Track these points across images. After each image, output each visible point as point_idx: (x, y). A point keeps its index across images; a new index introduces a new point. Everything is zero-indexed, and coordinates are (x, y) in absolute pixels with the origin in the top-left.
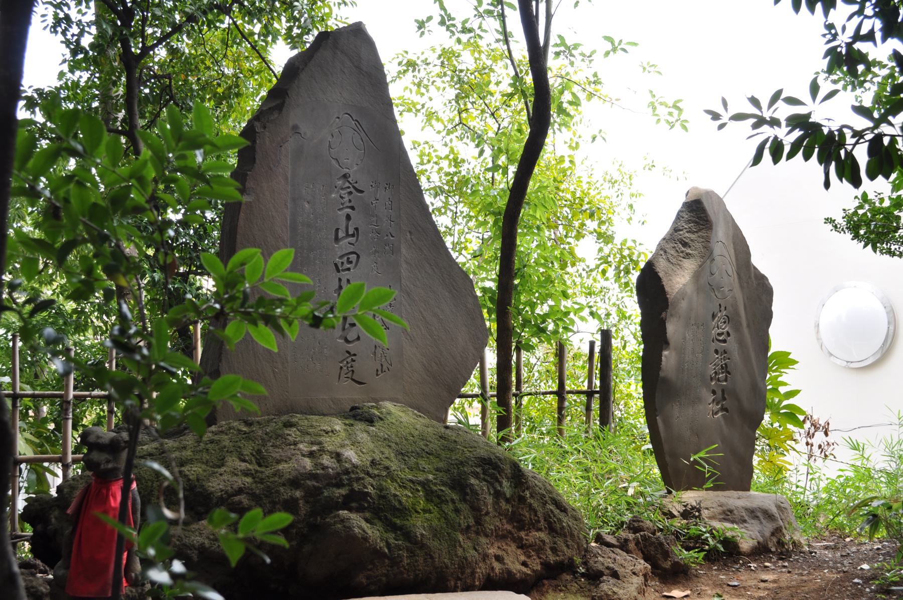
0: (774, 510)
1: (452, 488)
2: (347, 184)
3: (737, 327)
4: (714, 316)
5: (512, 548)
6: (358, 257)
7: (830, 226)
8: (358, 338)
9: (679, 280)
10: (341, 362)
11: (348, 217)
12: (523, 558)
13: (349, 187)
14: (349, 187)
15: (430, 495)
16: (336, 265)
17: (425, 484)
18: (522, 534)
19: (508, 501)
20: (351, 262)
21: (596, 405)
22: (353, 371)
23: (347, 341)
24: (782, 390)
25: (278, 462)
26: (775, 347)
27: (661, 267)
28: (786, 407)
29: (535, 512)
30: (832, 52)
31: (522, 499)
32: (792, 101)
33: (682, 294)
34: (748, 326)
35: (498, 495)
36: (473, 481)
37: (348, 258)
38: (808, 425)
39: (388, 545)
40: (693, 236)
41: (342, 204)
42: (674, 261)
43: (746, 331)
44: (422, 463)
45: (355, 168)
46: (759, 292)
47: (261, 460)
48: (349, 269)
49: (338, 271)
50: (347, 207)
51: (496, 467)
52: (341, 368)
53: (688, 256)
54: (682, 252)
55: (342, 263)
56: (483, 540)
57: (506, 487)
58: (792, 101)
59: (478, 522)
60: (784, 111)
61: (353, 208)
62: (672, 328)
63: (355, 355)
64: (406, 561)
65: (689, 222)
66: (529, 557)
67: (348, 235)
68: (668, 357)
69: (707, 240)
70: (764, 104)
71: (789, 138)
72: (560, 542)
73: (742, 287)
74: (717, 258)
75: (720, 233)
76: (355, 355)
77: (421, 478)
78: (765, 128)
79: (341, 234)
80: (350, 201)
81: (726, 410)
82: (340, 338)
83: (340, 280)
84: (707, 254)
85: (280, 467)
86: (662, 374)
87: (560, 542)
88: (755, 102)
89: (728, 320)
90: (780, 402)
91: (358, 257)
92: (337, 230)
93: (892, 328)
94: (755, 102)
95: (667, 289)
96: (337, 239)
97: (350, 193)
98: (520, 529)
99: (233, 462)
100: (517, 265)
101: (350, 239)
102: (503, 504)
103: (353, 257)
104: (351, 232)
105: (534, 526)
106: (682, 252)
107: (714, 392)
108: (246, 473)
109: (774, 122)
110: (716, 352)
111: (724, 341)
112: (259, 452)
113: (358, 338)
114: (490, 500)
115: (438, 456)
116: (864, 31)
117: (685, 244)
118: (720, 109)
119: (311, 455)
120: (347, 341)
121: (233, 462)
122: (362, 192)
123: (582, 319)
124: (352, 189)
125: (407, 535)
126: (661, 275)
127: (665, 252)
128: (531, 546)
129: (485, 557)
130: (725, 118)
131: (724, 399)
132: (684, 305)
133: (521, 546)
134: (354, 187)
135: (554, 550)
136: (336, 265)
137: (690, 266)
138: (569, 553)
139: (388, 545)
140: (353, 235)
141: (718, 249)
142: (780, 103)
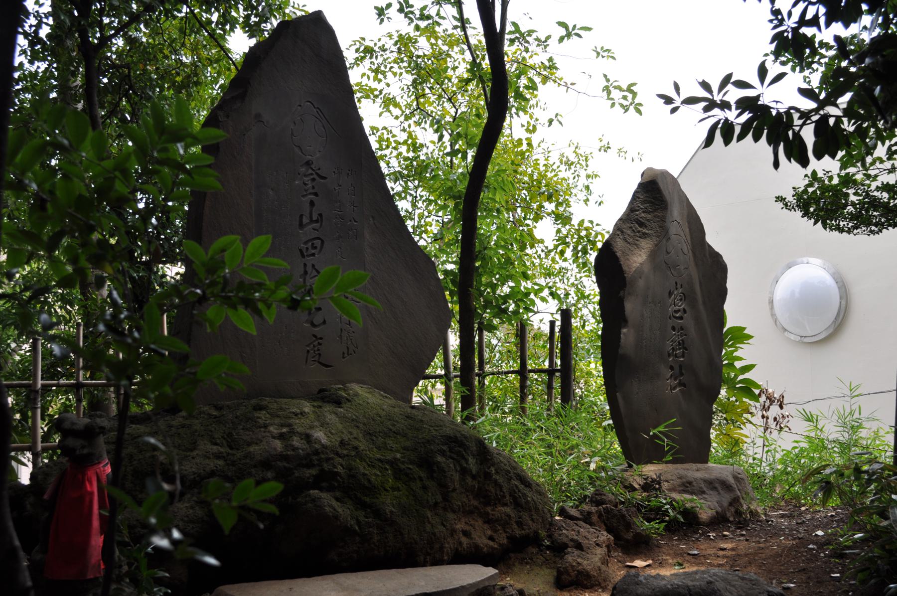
0: (732, 481)
1: (420, 466)
2: (310, 171)
3: (693, 304)
4: (670, 294)
5: (480, 523)
6: (323, 242)
7: (781, 205)
8: (324, 322)
9: (637, 259)
10: (308, 346)
11: (312, 203)
12: (489, 533)
13: (312, 174)
14: (312, 174)
15: (399, 474)
16: (301, 251)
17: (393, 463)
18: (489, 509)
19: (474, 477)
20: (315, 248)
21: (557, 384)
22: (320, 354)
23: (313, 325)
24: (738, 364)
25: (249, 444)
26: (730, 323)
27: (619, 245)
28: (741, 381)
29: (501, 487)
30: (778, 38)
31: (488, 475)
32: (742, 85)
33: (639, 272)
34: (704, 303)
35: (464, 471)
36: (440, 459)
37: (313, 244)
38: (763, 398)
39: (358, 522)
40: (649, 216)
41: (306, 191)
42: (631, 240)
43: (701, 307)
44: (390, 443)
45: (318, 155)
46: (713, 270)
47: (233, 444)
48: (313, 255)
49: (303, 256)
50: (310, 194)
51: (462, 444)
52: (308, 351)
53: (644, 236)
54: (639, 232)
55: (307, 249)
56: (451, 516)
57: (472, 464)
58: (742, 85)
59: (446, 498)
60: (734, 94)
61: (316, 194)
62: (631, 307)
63: (321, 338)
64: (376, 538)
65: (644, 202)
66: (496, 531)
67: (312, 221)
68: (627, 335)
69: (663, 220)
70: (715, 88)
71: (739, 119)
72: (525, 517)
73: (697, 265)
74: (673, 237)
75: (676, 212)
76: (321, 338)
77: (389, 456)
78: (716, 111)
79: (305, 220)
80: (313, 188)
81: (684, 385)
82: (307, 322)
83: (305, 265)
84: (663, 233)
85: (251, 449)
86: (621, 351)
87: (525, 517)
88: (705, 86)
89: (684, 297)
90: (736, 376)
91: (323, 242)
92: (301, 216)
93: (844, 303)
94: (705, 86)
95: (625, 268)
96: (301, 225)
97: (313, 180)
98: (487, 504)
99: (205, 446)
100: (478, 247)
101: (314, 225)
102: (469, 480)
103: (318, 243)
104: (315, 218)
105: (500, 501)
107: (672, 368)
108: (218, 456)
109: (725, 105)
110: (673, 329)
111: (681, 318)
112: (230, 435)
113: (324, 322)
114: (456, 477)
115: (405, 436)
116: (809, 16)
117: (641, 224)
118: (672, 94)
119: (281, 436)
120: (313, 325)
121: (205, 446)
122: (325, 178)
123: (543, 300)
124: (315, 176)
125: (377, 513)
126: (619, 254)
128: (497, 520)
129: (453, 532)
130: (678, 102)
131: (682, 374)
132: (641, 283)
133: (488, 521)
134: (317, 174)
135: (520, 524)
136: (301, 251)
137: (646, 245)
138: (534, 526)
139: (358, 522)
140: (317, 221)
141: (673, 229)
142: (730, 87)
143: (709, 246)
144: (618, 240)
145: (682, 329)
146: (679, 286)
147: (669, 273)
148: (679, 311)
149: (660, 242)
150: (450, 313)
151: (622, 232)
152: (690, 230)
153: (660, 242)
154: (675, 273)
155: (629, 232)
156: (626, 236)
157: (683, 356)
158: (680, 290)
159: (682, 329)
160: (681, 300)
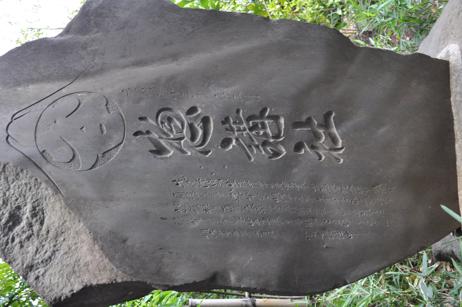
4: (159, 151)
34: (175, 57)
42: (48, 246)
54: (30, 225)
106: (30, 225)
111: (205, 121)
127: (31, 267)
143: (67, 30)
144: (46, 280)
145: (226, 121)
146: (142, 126)
147: (116, 154)
148: (191, 126)
149: (49, 181)
150: (185, 147)
151: (31, 267)
152: (32, 81)
153: (49, 181)
154: (117, 138)
155: (31, 248)
156: (39, 258)
157: (276, 118)
158: (151, 121)
159: (226, 121)
160: (170, 120)
